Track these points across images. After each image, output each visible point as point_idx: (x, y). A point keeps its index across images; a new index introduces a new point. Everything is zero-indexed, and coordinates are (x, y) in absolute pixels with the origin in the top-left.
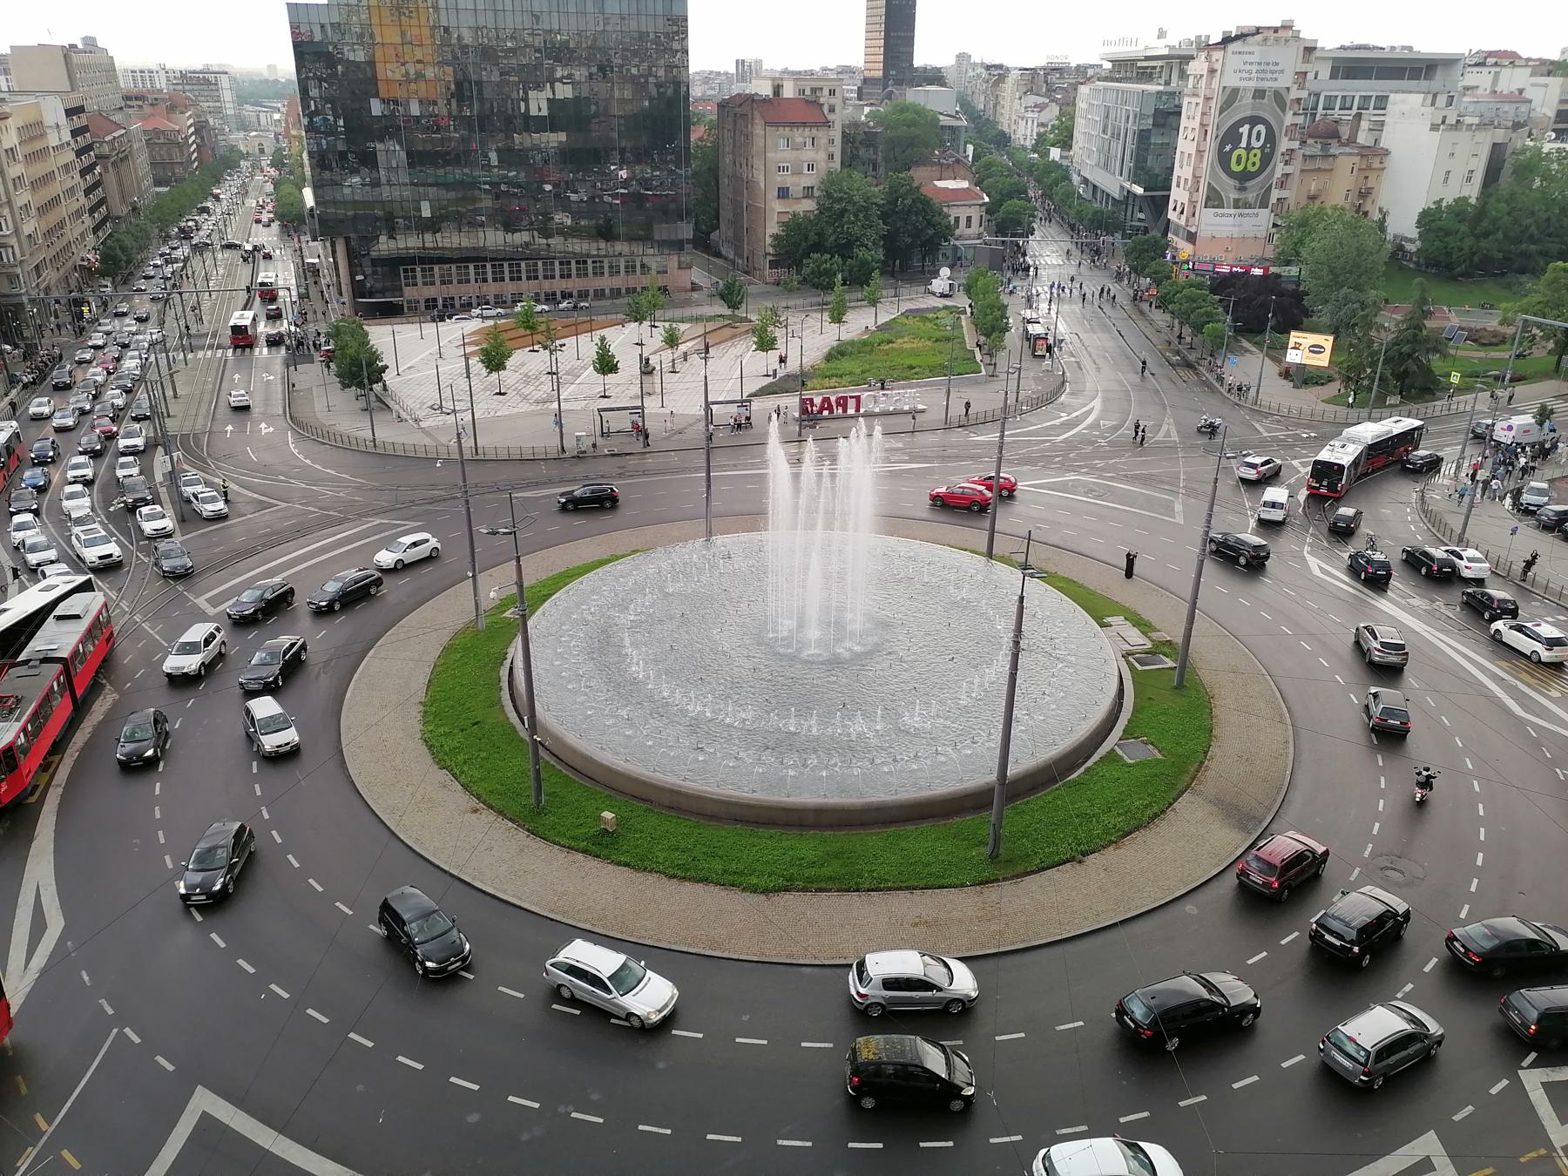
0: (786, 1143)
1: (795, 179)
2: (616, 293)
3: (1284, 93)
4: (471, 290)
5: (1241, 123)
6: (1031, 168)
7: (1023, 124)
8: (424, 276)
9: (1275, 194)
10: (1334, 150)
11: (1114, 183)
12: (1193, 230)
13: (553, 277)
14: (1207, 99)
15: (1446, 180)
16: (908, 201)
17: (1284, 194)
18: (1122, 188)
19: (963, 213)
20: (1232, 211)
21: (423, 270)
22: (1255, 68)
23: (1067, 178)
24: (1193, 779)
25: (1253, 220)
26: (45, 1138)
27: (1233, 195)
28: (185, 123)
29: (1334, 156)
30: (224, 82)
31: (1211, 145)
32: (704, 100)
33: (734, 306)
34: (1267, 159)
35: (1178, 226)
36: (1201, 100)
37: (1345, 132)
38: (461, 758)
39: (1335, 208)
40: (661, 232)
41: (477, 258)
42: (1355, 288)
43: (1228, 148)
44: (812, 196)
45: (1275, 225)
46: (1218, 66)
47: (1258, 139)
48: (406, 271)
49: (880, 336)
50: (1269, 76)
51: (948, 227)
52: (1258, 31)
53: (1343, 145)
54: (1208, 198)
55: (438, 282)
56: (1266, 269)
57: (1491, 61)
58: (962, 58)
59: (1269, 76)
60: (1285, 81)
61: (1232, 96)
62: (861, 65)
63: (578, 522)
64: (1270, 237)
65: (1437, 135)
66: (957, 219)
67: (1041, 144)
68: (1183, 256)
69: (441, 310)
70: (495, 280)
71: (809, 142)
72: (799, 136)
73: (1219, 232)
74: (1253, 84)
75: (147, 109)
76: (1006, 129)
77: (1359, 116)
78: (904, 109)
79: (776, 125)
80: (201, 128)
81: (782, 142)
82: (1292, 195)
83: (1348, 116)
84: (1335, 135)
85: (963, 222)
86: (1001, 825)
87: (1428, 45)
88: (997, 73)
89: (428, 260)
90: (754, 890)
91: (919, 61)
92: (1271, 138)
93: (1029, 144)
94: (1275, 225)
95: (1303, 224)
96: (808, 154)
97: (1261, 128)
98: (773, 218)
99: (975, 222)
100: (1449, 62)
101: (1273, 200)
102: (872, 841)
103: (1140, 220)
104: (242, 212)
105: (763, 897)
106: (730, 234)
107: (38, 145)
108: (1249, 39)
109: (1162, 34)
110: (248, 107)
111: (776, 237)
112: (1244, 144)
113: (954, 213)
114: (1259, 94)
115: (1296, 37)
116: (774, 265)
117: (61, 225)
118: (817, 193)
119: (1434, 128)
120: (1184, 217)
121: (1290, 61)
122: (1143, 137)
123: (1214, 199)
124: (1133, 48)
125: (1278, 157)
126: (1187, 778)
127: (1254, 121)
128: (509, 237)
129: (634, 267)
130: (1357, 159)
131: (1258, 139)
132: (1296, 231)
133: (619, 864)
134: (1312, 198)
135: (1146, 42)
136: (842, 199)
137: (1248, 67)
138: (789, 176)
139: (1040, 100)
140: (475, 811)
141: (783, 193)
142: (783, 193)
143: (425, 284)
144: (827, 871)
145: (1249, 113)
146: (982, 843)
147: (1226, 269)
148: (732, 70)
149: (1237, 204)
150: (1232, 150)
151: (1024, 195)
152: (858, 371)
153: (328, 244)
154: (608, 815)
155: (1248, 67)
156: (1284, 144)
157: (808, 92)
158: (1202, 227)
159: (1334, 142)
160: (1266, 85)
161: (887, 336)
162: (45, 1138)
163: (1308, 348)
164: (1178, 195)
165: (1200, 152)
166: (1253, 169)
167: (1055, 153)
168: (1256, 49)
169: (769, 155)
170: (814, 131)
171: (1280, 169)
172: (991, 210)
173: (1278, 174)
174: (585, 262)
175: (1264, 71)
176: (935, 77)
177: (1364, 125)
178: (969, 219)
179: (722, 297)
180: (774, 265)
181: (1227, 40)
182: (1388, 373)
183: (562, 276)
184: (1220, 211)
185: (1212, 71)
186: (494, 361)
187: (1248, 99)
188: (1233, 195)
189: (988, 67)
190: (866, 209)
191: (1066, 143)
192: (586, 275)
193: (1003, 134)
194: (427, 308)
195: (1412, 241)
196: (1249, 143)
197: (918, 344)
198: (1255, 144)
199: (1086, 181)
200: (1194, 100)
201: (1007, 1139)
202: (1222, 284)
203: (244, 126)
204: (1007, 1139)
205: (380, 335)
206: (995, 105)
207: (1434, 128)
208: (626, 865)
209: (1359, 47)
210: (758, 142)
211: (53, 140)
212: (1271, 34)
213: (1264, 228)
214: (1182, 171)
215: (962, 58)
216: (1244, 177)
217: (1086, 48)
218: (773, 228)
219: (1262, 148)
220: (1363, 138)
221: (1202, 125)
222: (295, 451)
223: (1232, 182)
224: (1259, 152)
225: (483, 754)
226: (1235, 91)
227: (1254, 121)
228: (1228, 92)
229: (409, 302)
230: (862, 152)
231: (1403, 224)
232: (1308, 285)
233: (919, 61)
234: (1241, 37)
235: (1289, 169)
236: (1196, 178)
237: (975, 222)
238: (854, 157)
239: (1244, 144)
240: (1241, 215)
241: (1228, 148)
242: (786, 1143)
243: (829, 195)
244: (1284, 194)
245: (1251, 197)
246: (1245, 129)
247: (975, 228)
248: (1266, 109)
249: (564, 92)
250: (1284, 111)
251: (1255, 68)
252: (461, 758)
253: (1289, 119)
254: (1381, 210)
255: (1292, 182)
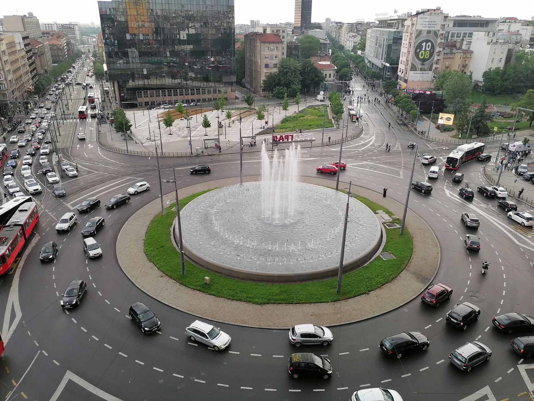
0: (268, 390)
1: (271, 61)
2: (210, 100)
3: (437, 32)
4: (161, 99)
5: (423, 42)
6: (351, 57)
7: (348, 42)
8: (144, 94)
9: (434, 66)
10: (454, 51)
11: (380, 62)
12: (406, 78)
13: (188, 94)
14: (411, 34)
15: (492, 61)
16: (309, 69)
17: (437, 66)
18: (382, 64)
19: (328, 73)
20: (420, 72)
21: (144, 92)
22: (427, 23)
23: (363, 61)
24: (406, 266)
25: (427, 75)
26: (15, 388)
27: (420, 67)
28: (63, 42)
29: (454, 53)
30: (76, 28)
31: (412, 50)
32: (240, 34)
33: (250, 104)
34: (431, 54)
35: (401, 77)
36: (409, 34)
37: (458, 45)
38: (157, 258)
39: (455, 71)
40: (225, 79)
41: (162, 88)
42: (462, 98)
43: (418, 50)
44: (277, 67)
45: (434, 77)
46: (415, 23)
47: (428, 47)
48: (138, 92)
49: (300, 115)
50: (432, 26)
51: (323, 77)
52: (428, 10)
53: (457, 49)
54: (411, 68)
55: (149, 96)
56: (431, 92)
57: (508, 21)
58: (328, 20)
59: (432, 26)
60: (438, 27)
61: (420, 33)
62: (293, 22)
63: (197, 178)
64: (433, 81)
65: (489, 46)
66: (326, 75)
67: (355, 49)
68: (403, 87)
69: (150, 106)
70: (169, 95)
71: (276, 48)
72: (272, 46)
73: (415, 79)
74: (427, 29)
75: (50, 37)
76: (343, 44)
77: (463, 40)
78: (308, 37)
79: (264, 42)
80: (68, 44)
81: (266, 48)
82: (440, 66)
83: (459, 39)
84: (455, 46)
85: (328, 76)
86: (341, 281)
87: (486, 15)
88: (340, 25)
89: (146, 89)
90: (257, 303)
91: (313, 21)
92: (433, 47)
93: (350, 49)
94: (434, 77)
95: (444, 76)
96: (275, 53)
97: (430, 43)
98: (263, 74)
99: (332, 76)
100: (493, 21)
101: (434, 68)
102: (297, 287)
103: (388, 75)
104: (82, 72)
105: (260, 306)
106: (249, 80)
107: (13, 50)
108: (426, 13)
109: (396, 12)
110: (84, 36)
111: (264, 81)
112: (424, 49)
113: (325, 73)
114: (429, 32)
115: (442, 13)
116: (263, 90)
117: (21, 77)
118: (278, 66)
119: (488, 43)
120: (403, 74)
121: (439, 21)
122: (389, 47)
123: (413, 68)
124: (386, 16)
125: (435, 53)
126: (404, 265)
127: (427, 41)
128: (173, 81)
129: (216, 91)
130: (462, 54)
131: (428, 47)
132: (441, 79)
133: (211, 295)
134: (447, 68)
135: (390, 14)
136: (287, 68)
137: (425, 23)
138: (269, 60)
139: (354, 34)
140: (162, 277)
141: (267, 66)
142: (267, 66)
143: (145, 97)
144: (282, 297)
145: (425, 39)
146: (334, 288)
147: (417, 92)
148: (249, 24)
149: (421, 70)
150: (420, 51)
151: (349, 66)
152: (292, 126)
153: (112, 83)
154: (207, 278)
155: (425, 23)
156: (437, 49)
157: (275, 31)
158: (410, 77)
159: (454, 48)
160: (431, 29)
161: (302, 115)
162: (15, 388)
163: (446, 119)
164: (401, 66)
165: (409, 52)
166: (427, 58)
167: (359, 52)
168: (428, 17)
169: (262, 53)
170: (277, 45)
171: (436, 58)
172: (337, 71)
173: (435, 59)
174: (199, 89)
175: (430, 24)
176: (318, 26)
177: (465, 43)
178: (330, 75)
179: (246, 101)
180: (263, 90)
181: (418, 14)
182: (473, 127)
183: (191, 94)
184: (415, 72)
185: (413, 24)
186: (168, 123)
187: (425, 34)
188: (420, 67)
189: (337, 23)
190: (295, 71)
191: (363, 49)
192: (200, 94)
193: (342, 46)
194: (145, 105)
195: (481, 82)
196: (425, 49)
197: (313, 117)
198: (427, 49)
199: (370, 62)
200: (407, 34)
201: (343, 388)
202: (416, 97)
203: (83, 43)
204: (343, 388)
205: (130, 114)
206: (339, 36)
207: (488, 43)
208: (213, 295)
209: (463, 16)
210: (258, 48)
211: (18, 48)
212: (433, 12)
213: (430, 78)
214: (403, 58)
215: (328, 20)
216: (424, 60)
217: (370, 16)
218: (263, 78)
219: (430, 50)
220: (464, 47)
221: (409, 43)
222: (101, 154)
223: (420, 62)
224: (429, 52)
225: (165, 257)
226: (421, 31)
227: (427, 41)
228: (418, 31)
229: (139, 103)
230: (294, 52)
231: (478, 76)
232: (446, 97)
233: (313, 21)
234: (423, 12)
235: (439, 58)
236: (407, 61)
237: (332, 76)
238: (291, 54)
239: (424, 49)
240: (423, 73)
241: (418, 50)
242: (268, 390)
243: (282, 67)
244: (437, 66)
245: (426, 67)
246: (424, 44)
247: (332, 78)
248: (431, 37)
249: (192, 31)
250: (437, 38)
251: (427, 23)
252: (157, 258)
253: (439, 41)
254: (470, 72)
255: (440, 62)
